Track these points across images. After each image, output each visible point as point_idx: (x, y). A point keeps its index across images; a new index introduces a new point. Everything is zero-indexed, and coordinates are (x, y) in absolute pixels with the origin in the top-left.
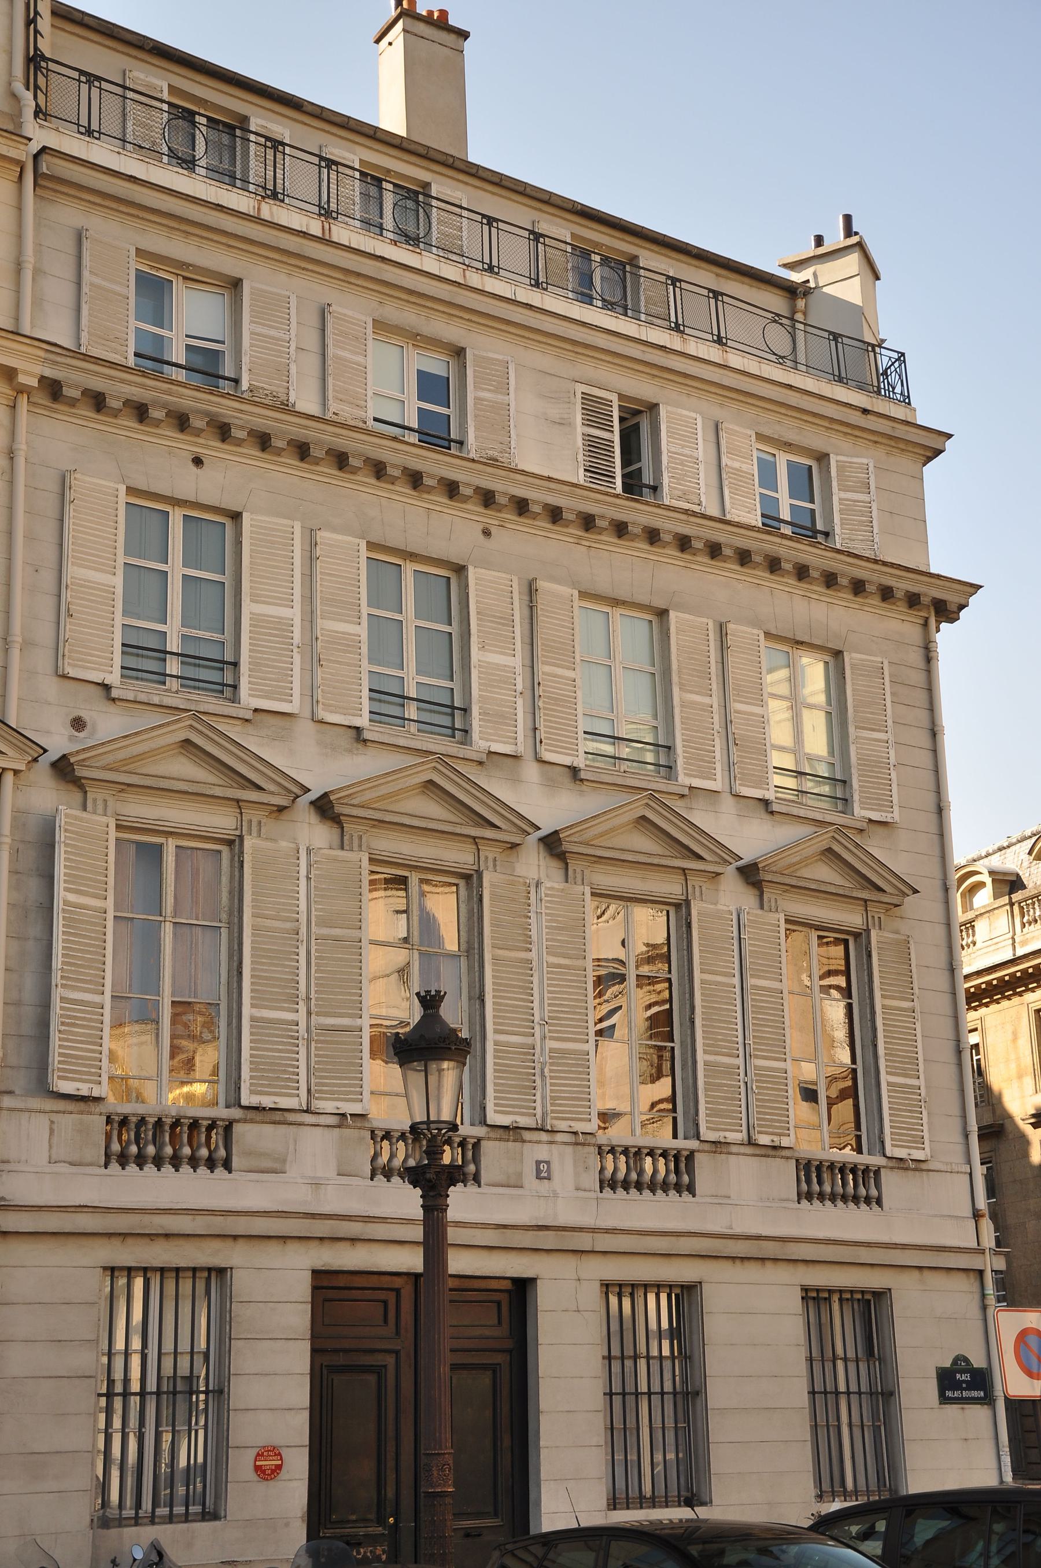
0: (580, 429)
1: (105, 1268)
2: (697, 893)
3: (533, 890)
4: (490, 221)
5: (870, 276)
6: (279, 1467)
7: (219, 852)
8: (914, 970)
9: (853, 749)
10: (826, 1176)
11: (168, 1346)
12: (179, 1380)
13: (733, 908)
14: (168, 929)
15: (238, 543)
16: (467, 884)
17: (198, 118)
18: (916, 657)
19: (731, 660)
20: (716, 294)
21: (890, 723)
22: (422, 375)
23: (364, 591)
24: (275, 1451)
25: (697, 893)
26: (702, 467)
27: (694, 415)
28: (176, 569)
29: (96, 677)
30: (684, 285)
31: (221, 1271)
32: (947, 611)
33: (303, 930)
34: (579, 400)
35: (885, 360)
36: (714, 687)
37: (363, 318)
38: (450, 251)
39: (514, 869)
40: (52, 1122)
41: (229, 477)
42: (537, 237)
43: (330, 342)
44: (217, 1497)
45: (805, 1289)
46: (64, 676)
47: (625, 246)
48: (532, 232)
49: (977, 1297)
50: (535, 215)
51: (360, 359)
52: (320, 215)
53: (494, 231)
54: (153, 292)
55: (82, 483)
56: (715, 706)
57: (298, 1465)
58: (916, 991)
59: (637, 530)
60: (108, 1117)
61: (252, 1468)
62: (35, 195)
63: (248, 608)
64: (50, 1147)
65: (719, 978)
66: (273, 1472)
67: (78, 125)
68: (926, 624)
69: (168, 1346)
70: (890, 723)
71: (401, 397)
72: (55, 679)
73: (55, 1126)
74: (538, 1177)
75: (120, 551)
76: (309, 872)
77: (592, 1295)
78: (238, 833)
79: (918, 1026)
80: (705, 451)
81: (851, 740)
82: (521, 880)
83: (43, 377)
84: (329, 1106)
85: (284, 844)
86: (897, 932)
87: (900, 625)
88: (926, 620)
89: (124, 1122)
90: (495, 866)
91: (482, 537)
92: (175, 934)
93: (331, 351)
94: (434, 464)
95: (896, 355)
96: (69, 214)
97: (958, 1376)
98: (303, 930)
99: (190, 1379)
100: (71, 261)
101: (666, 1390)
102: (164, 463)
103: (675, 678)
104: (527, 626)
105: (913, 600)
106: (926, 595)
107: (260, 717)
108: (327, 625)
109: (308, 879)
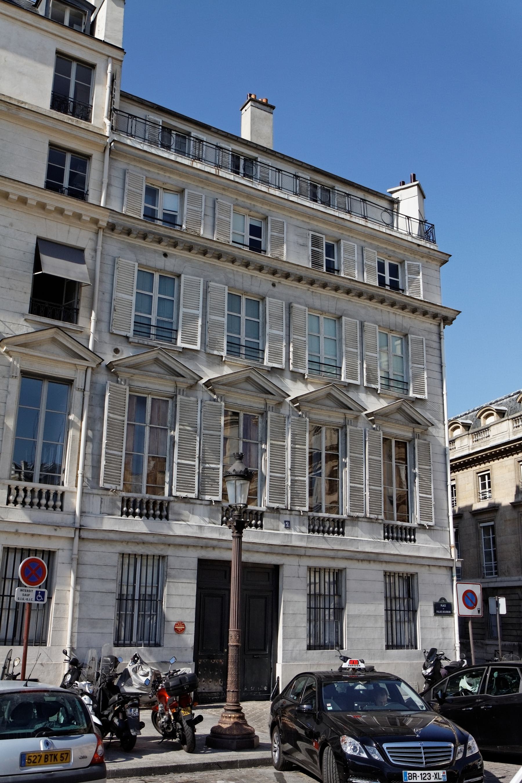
0: (310, 248)
1: (120, 554)
2: (350, 423)
3: (287, 419)
4: (279, 171)
5: (422, 198)
6: (184, 629)
7: (168, 401)
8: (431, 454)
9: (410, 371)
10: (395, 530)
11: (143, 584)
12: (147, 596)
13: (363, 429)
14: (147, 429)
15: (179, 286)
16: (262, 416)
17: (173, 132)
18: (435, 337)
19: (365, 336)
20: (364, 200)
21: (425, 362)
22: (251, 226)
23: (226, 305)
24: (182, 623)
25: (350, 423)
26: (356, 264)
27: (354, 244)
28: (156, 295)
30: (352, 197)
31: (164, 557)
32: (447, 320)
33: (199, 431)
34: (310, 237)
35: (427, 227)
36: (359, 345)
37: (230, 204)
38: (265, 182)
39: (280, 411)
40: (102, 499)
41: (177, 261)
43: (217, 212)
44: (160, 639)
45: (385, 573)
46: (112, 333)
47: (329, 182)
48: (294, 175)
49: (450, 576)
50: (297, 170)
51: (228, 219)
52: (215, 166)
53: (280, 174)
54: (152, 193)
55: (122, 261)
56: (359, 353)
57: (191, 628)
58: (432, 462)
60: (62, 510)
61: (173, 629)
62: (110, 158)
63: (182, 310)
64: (101, 508)
65: (357, 455)
66: (181, 631)
67: (127, 133)
68: (439, 325)
69: (143, 584)
70: (425, 362)
71: (243, 234)
72: (108, 334)
73: (103, 500)
74: (289, 522)
75: (135, 287)
76: (201, 409)
77: (303, 571)
78: (175, 394)
79: (432, 476)
80: (358, 258)
81: (410, 367)
82: (282, 415)
83: (108, 222)
84: (207, 497)
85: (192, 399)
86: (425, 440)
87: (430, 324)
88: (440, 324)
89: (128, 500)
90: (272, 410)
91: (272, 286)
92: (150, 431)
93: (217, 216)
94: (253, 256)
95: (430, 226)
97: (441, 605)
98: (199, 431)
99: (151, 595)
100: (122, 181)
102: (154, 257)
103: (344, 342)
104: (288, 320)
105: (435, 316)
106: (440, 314)
107: (185, 351)
108: (212, 317)
109: (201, 412)
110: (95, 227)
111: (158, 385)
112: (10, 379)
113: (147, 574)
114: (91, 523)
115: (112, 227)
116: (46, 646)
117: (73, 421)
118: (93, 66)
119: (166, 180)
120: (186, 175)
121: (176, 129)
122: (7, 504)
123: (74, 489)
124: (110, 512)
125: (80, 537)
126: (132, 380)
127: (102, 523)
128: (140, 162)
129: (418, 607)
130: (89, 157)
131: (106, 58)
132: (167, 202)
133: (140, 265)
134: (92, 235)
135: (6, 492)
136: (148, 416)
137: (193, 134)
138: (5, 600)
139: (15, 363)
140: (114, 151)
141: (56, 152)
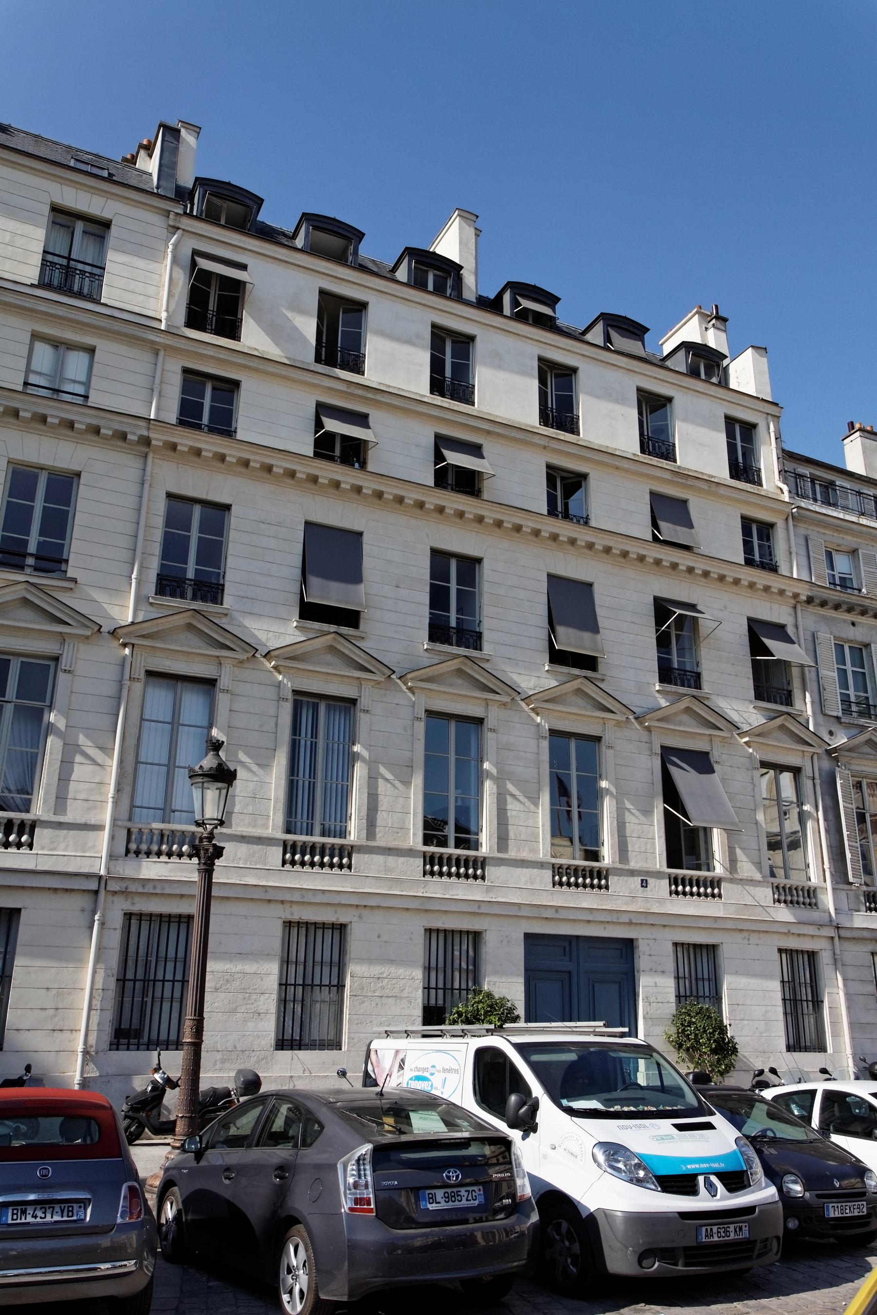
29: (835, 714)
38: (845, 508)
42: (860, 493)
46: (825, 715)
59: (776, 591)
89: (560, 867)
96: (803, 530)
101: (127, 977)
110: (793, 601)
111: (580, 720)
112: (541, 740)
113: (325, 946)
114: (845, 922)
115: (810, 600)
116: (341, 1049)
117: (487, 771)
118: (754, 426)
119: (840, 542)
120: (860, 534)
121: (819, 478)
122: (283, 866)
123: (823, 884)
124: (856, 908)
125: (839, 937)
126: (850, 764)
127: (852, 920)
128: (818, 525)
129: (824, 997)
130: (772, 526)
131: (765, 416)
132: (842, 564)
133: (835, 638)
134: (791, 611)
135: (281, 849)
136: (453, 743)
137: (838, 483)
138: (137, 987)
139: (285, 681)
140: (797, 518)
141: (193, 379)
